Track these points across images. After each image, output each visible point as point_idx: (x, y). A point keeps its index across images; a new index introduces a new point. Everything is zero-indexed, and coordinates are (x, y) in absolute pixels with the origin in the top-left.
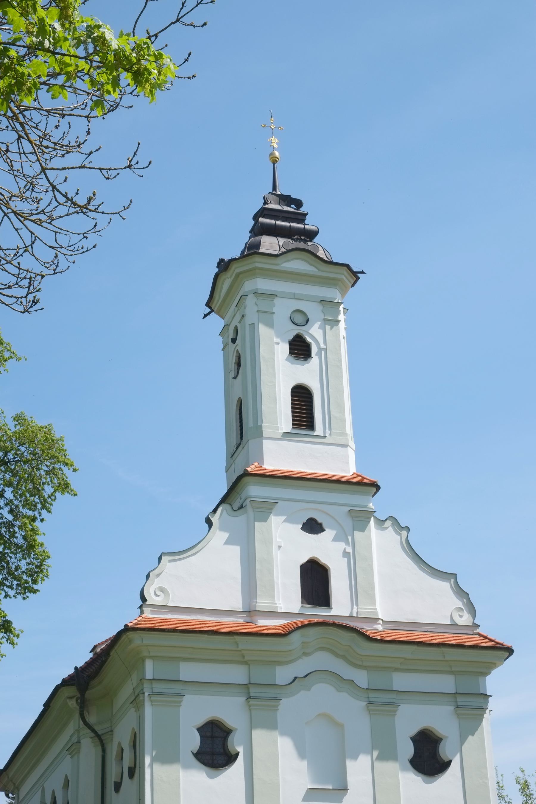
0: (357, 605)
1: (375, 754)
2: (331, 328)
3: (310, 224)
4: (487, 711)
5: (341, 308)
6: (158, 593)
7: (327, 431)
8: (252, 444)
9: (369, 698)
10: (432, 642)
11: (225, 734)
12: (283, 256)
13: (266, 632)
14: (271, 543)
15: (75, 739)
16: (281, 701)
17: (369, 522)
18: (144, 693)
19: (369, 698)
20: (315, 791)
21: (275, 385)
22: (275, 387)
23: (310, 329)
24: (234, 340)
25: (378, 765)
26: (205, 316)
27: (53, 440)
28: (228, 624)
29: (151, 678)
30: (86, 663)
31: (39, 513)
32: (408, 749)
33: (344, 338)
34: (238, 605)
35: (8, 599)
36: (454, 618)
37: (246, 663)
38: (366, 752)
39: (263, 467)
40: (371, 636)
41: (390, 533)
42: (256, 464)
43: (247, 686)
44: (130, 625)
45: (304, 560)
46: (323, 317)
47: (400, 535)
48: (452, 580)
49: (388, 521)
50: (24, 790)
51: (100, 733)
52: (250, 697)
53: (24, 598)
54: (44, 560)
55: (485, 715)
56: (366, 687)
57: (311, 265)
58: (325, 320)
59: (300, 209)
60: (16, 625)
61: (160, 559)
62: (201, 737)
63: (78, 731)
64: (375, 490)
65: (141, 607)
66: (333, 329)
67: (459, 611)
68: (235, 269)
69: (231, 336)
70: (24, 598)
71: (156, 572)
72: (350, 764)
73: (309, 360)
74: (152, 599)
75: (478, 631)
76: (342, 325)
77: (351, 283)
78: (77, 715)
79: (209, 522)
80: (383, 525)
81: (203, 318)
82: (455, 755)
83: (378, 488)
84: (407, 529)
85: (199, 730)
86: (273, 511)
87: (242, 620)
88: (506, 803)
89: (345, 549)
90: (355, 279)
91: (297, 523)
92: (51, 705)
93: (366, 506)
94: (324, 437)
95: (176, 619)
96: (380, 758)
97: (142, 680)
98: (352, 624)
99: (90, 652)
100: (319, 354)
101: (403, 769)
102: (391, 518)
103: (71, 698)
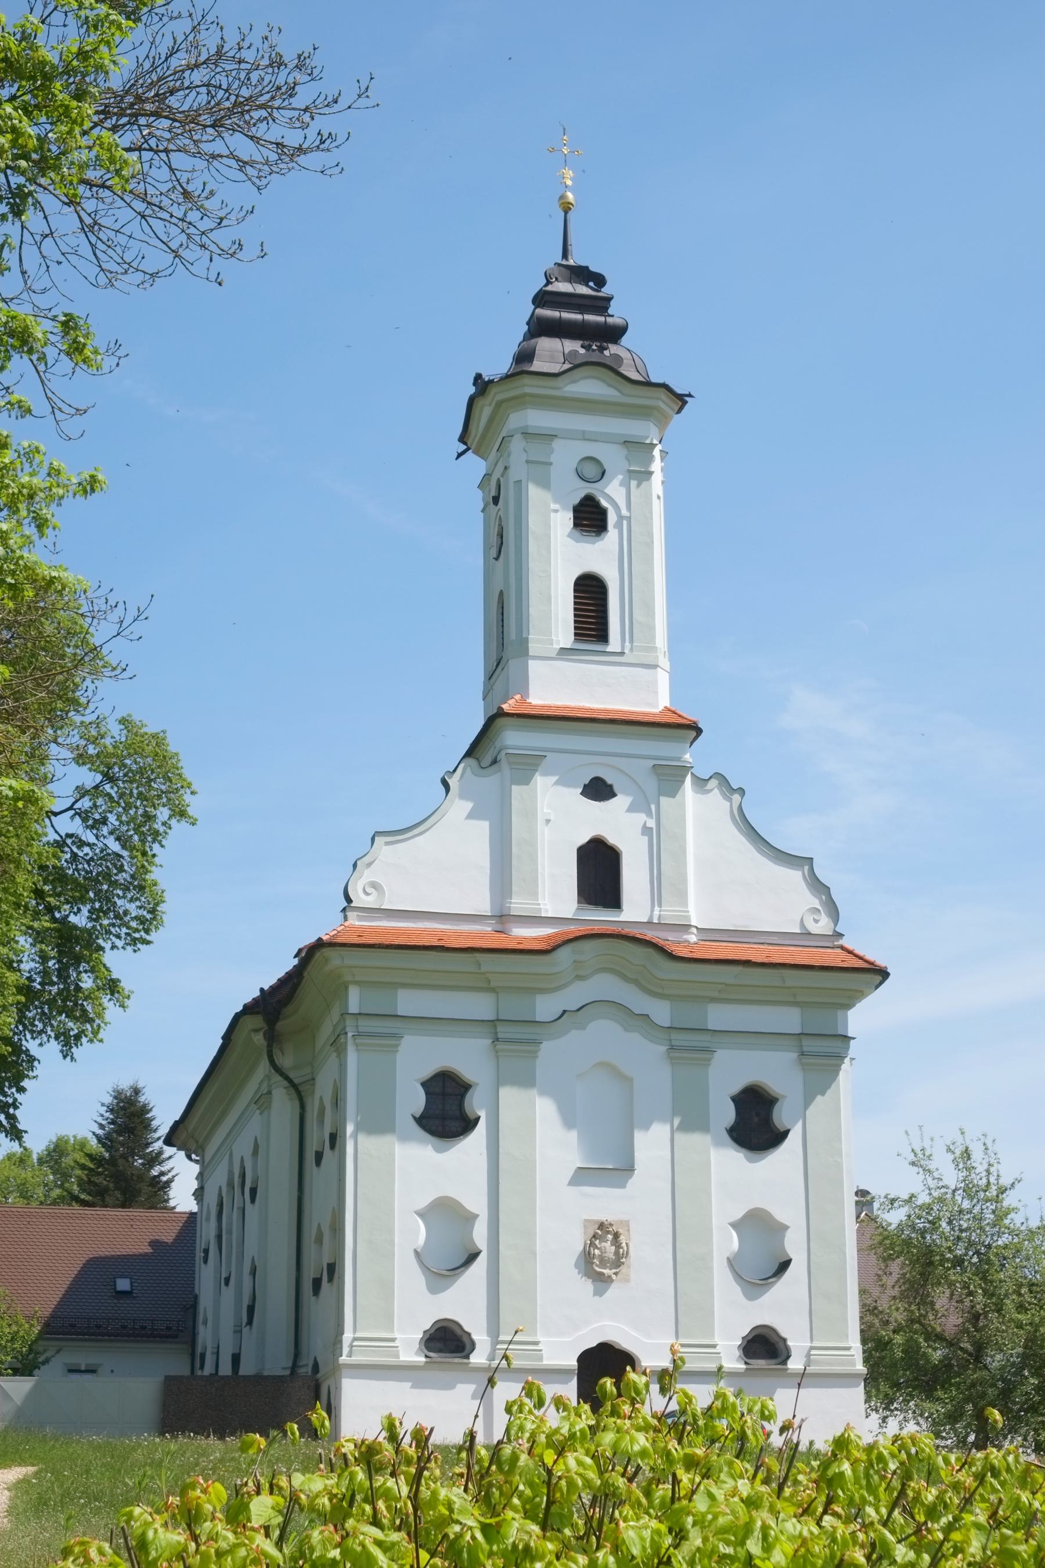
0: (660, 905)
1: (677, 1121)
2: (638, 486)
3: (617, 313)
4: (847, 1060)
5: (656, 452)
6: (369, 890)
7: (627, 644)
8: (513, 665)
9: (671, 1040)
10: (766, 960)
11: (463, 1090)
12: (564, 375)
13: (520, 947)
14: (534, 815)
15: (264, 1089)
16: (542, 1045)
17: (683, 782)
18: (346, 1033)
19: (671, 1040)
20: (587, 1170)
21: (550, 576)
22: (550, 579)
23: (606, 487)
24: (496, 500)
25: (680, 1137)
26: (460, 455)
27: (164, 757)
28: (469, 935)
29: (356, 1011)
30: (279, 980)
31: (150, 847)
32: (729, 1115)
33: (659, 497)
34: (483, 905)
35: (115, 950)
36: (806, 924)
37: (493, 990)
38: (662, 1119)
39: (528, 701)
40: (674, 953)
41: (715, 798)
42: (518, 697)
43: (493, 1023)
44: (325, 938)
45: (584, 839)
46: (627, 467)
47: (730, 800)
48: (806, 868)
49: (712, 780)
50: (210, 1150)
51: (296, 1081)
52: (498, 1039)
53: (135, 951)
54: (157, 904)
55: (843, 1067)
56: (667, 1024)
57: (610, 385)
58: (629, 471)
59: (602, 290)
60: (125, 985)
61: (373, 840)
62: (427, 1094)
63: (268, 1077)
64: (694, 734)
65: (344, 910)
66: (642, 486)
67: (813, 913)
68: (495, 394)
69: (493, 493)
70: (135, 951)
71: (366, 860)
72: (639, 1137)
73: (603, 535)
74: (360, 899)
75: (841, 942)
76: (657, 478)
77: (673, 410)
78: (266, 1057)
79: (445, 784)
80: (706, 786)
81: (457, 459)
82: (795, 1123)
83: (699, 731)
84: (741, 791)
85: (423, 1084)
86: (540, 769)
87: (490, 929)
88: (934, 1179)
89: (645, 823)
90: (680, 403)
91: (575, 786)
92: (232, 1038)
93: (679, 759)
94: (622, 654)
95: (394, 928)
96: (686, 1127)
97: (344, 1014)
98: (650, 935)
99: (295, 957)
100: (619, 526)
101: (718, 1144)
102: (717, 775)
103: (256, 1031)
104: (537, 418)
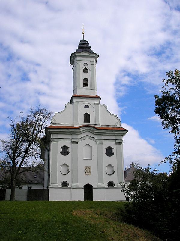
104: (78, 58)
